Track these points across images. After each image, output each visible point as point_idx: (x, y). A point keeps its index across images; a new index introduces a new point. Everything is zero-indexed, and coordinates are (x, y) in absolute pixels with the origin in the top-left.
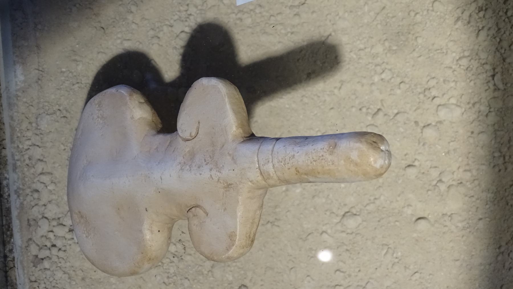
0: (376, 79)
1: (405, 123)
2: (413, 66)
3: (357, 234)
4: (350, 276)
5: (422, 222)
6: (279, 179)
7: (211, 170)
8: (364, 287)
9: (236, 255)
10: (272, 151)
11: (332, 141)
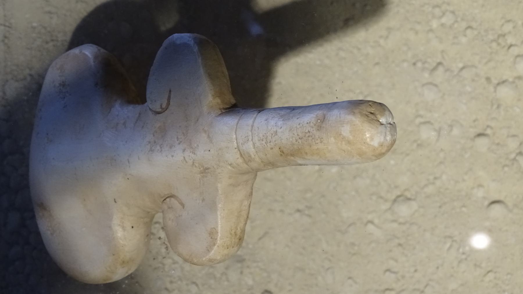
0: (435, 24)
1: (473, 80)
2: (483, 6)
3: (412, 224)
4: (403, 277)
5: (496, 207)
6: (262, 162)
7: (184, 150)
8: (423, 292)
9: (219, 258)
10: (252, 126)
11: (320, 113)
